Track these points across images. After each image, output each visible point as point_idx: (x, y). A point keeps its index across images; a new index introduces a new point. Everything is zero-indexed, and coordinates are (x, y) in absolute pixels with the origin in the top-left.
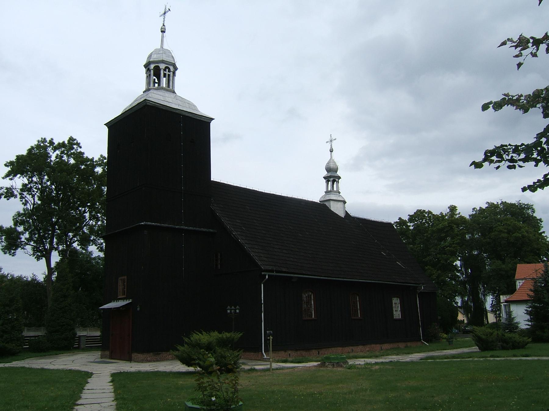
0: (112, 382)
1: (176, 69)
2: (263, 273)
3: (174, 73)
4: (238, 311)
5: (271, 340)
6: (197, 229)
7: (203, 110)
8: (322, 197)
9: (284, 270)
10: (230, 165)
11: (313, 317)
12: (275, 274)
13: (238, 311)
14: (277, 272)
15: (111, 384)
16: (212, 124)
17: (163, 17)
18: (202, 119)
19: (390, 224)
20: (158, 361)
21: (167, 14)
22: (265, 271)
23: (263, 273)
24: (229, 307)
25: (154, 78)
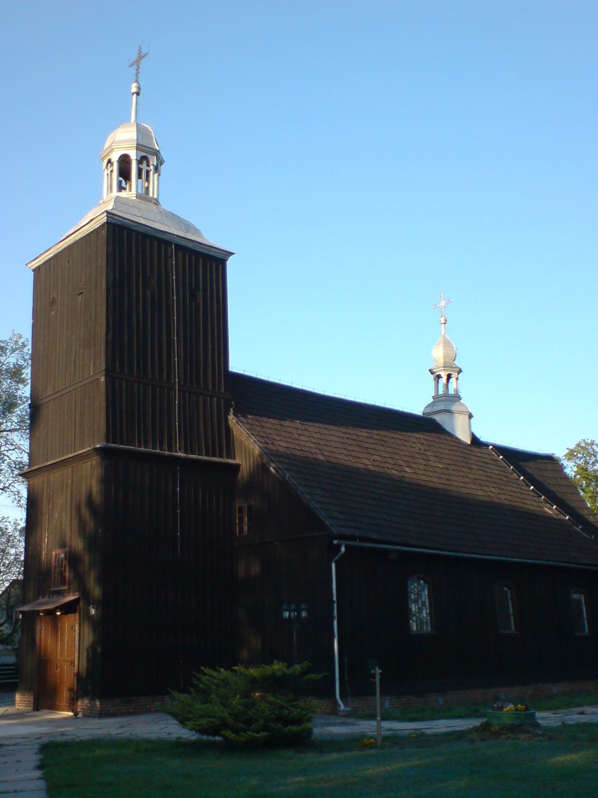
0: (40, 767)
1: (160, 162)
2: (335, 542)
3: (157, 169)
4: (304, 614)
5: (378, 677)
6: (204, 458)
7: (212, 235)
8: (429, 406)
9: (375, 536)
10: (261, 345)
11: (513, 628)
12: (358, 543)
13: (304, 614)
14: (362, 539)
15: (39, 773)
16: (230, 264)
17: (134, 68)
18: (211, 253)
19: (550, 460)
20: (129, 714)
21: (144, 62)
22: (342, 537)
23: (335, 542)
24: (285, 607)
25: (121, 179)
